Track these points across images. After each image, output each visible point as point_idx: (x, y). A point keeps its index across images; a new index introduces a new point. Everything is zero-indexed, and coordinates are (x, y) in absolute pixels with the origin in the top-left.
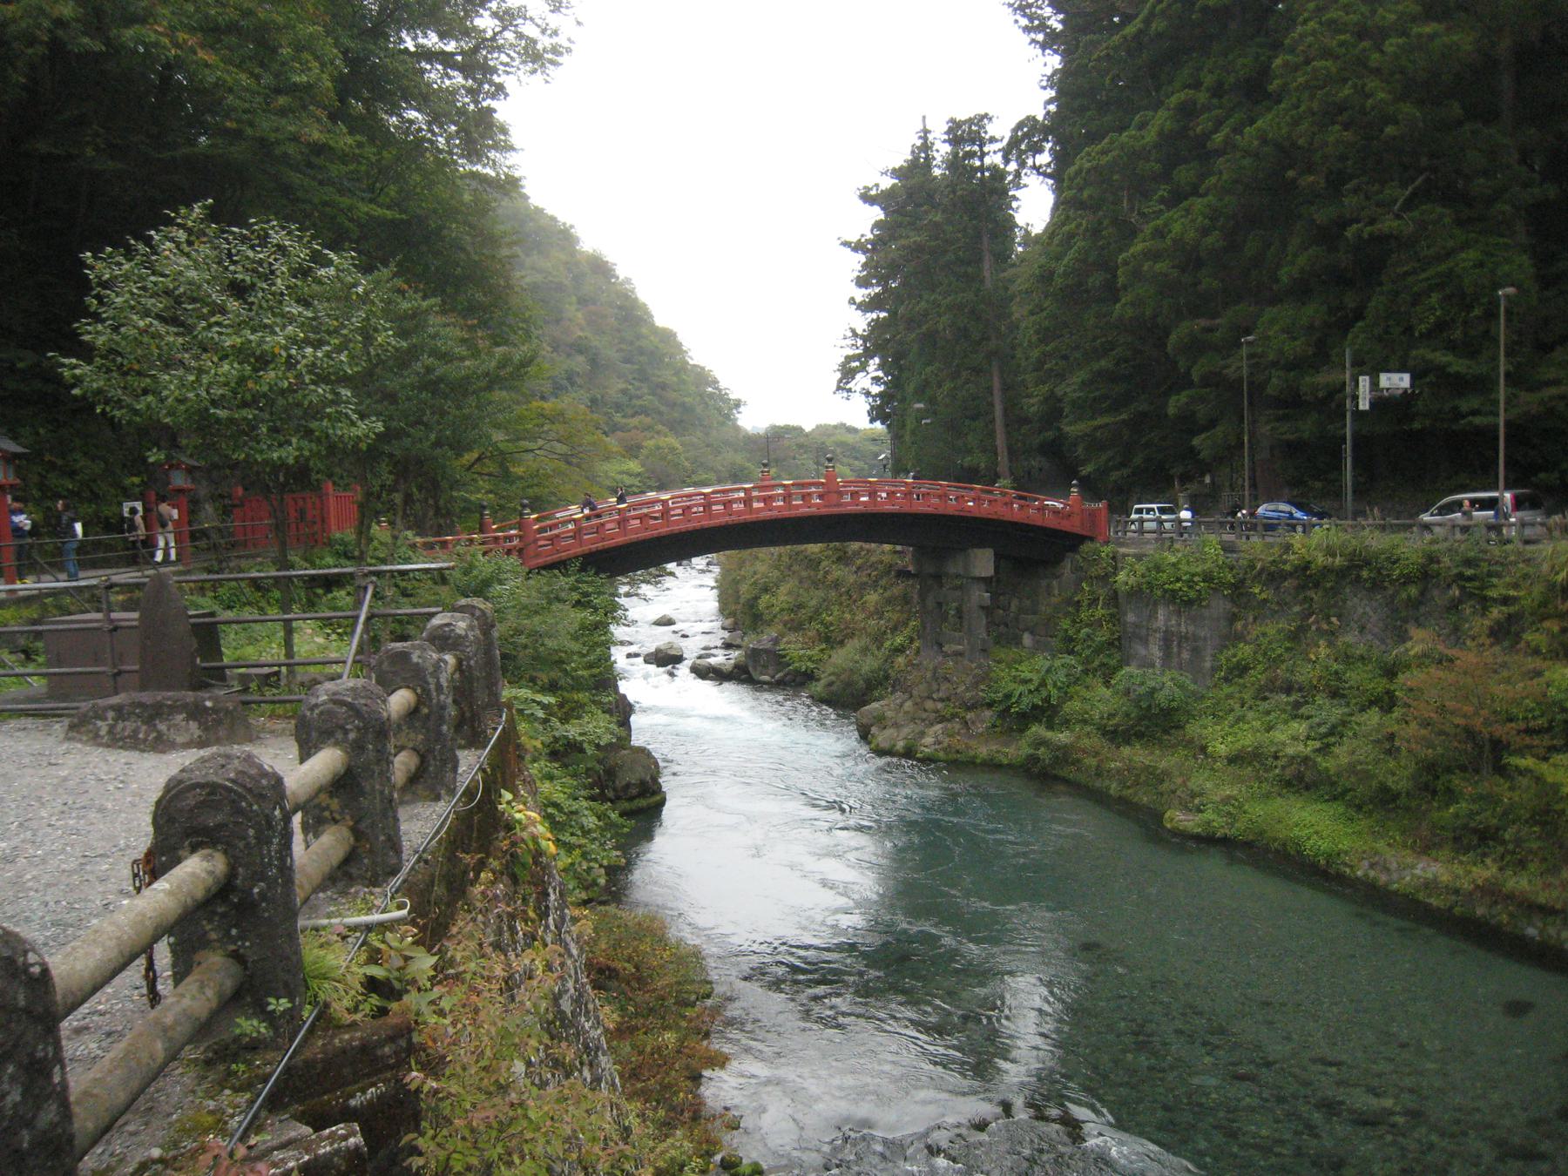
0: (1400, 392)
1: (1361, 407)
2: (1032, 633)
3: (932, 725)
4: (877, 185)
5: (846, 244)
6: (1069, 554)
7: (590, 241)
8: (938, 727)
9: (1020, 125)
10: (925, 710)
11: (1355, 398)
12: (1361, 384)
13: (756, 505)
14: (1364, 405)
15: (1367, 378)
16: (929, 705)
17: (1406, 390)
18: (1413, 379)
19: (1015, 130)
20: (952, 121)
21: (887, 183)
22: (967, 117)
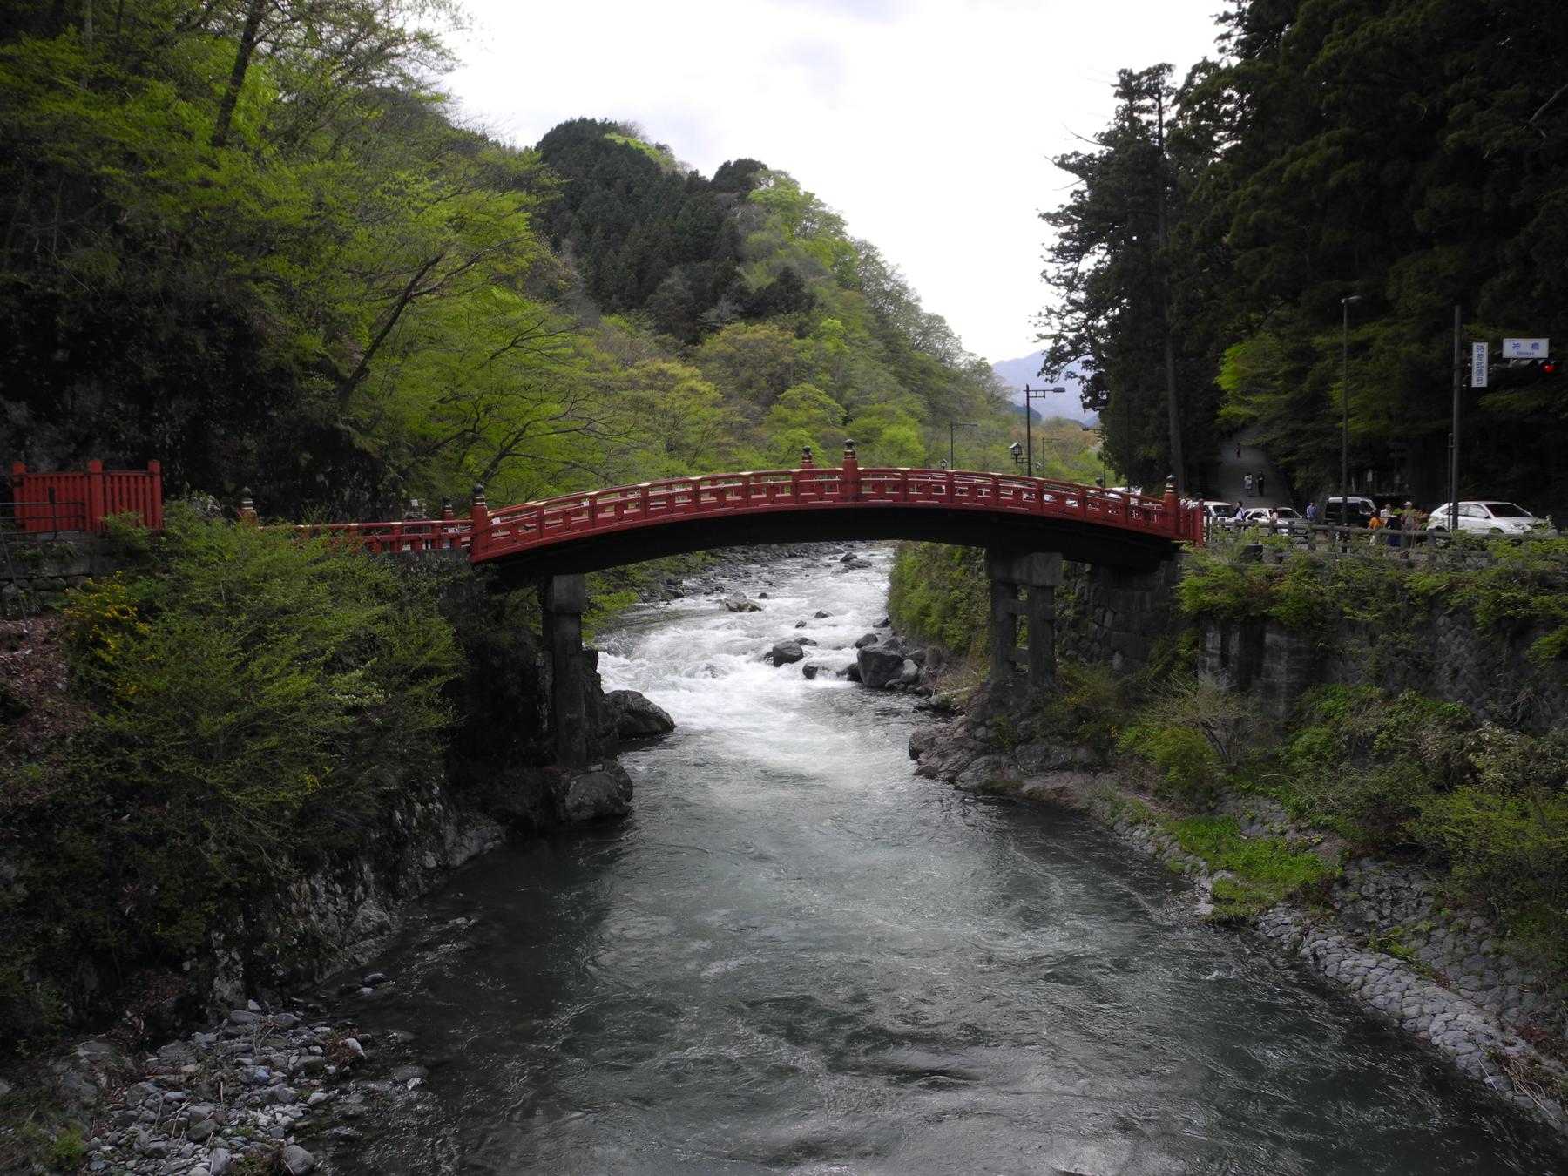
0: (1529, 362)
1: (1475, 384)
2: (1122, 653)
3: (979, 755)
4: (1076, 154)
5: (1047, 217)
6: (1164, 562)
7: (855, 231)
8: (983, 759)
9: (1196, 69)
10: (975, 738)
11: (1467, 372)
12: (1475, 353)
13: (705, 499)
14: (1479, 380)
15: (1485, 345)
16: (980, 732)
17: (1535, 361)
18: (1551, 344)
19: (1191, 77)
20: (1124, 71)
21: (1098, 150)
22: (1144, 68)
